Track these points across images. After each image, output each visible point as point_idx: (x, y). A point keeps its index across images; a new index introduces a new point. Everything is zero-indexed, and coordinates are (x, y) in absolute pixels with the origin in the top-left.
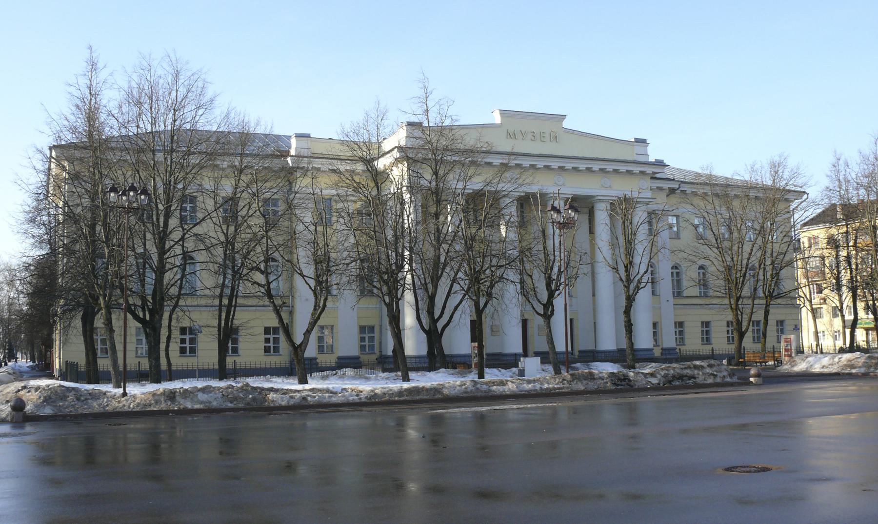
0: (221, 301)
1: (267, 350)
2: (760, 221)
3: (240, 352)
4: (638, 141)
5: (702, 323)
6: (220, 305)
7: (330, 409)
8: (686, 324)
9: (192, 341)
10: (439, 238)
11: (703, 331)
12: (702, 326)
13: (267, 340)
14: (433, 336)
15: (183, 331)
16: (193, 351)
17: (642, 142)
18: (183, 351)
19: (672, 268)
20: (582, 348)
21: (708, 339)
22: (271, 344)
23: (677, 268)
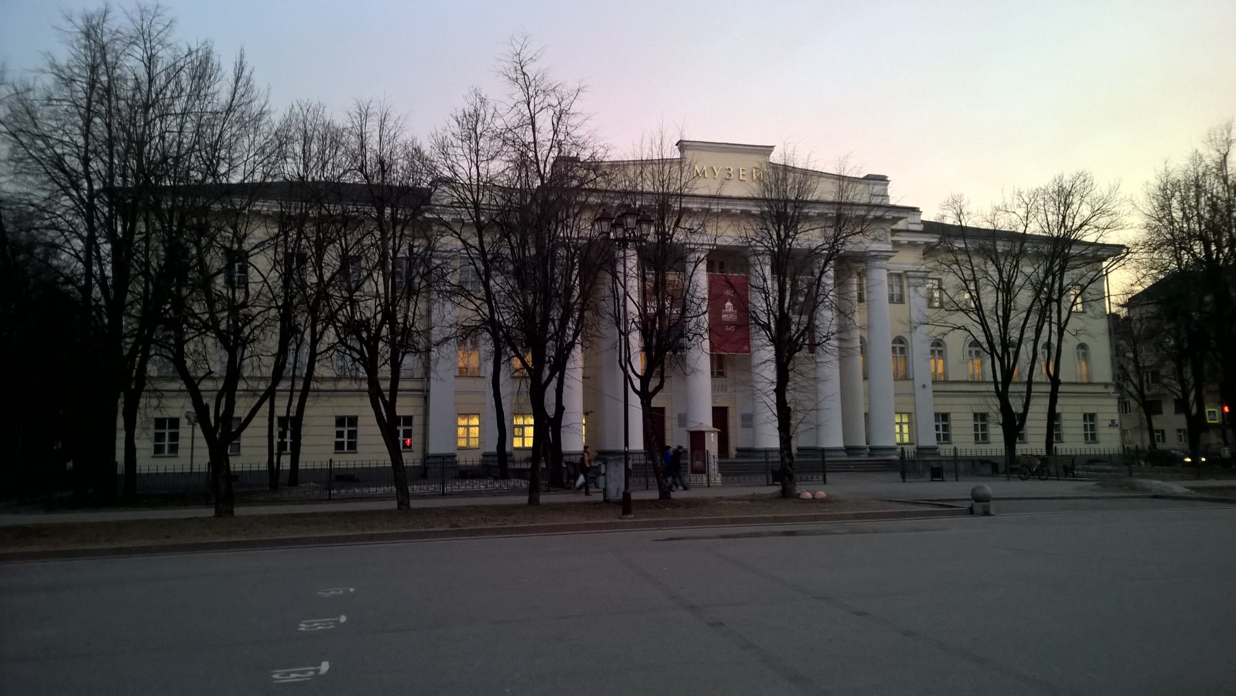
0: (293, 385)
1: (339, 446)
2: (304, 242)
3: (359, 448)
4: (869, 178)
5: (1085, 416)
6: (292, 391)
7: (565, 520)
8: (952, 416)
9: (353, 434)
10: (429, 300)
11: (976, 426)
12: (1085, 420)
13: (340, 434)
14: (901, 428)
15: (160, 423)
16: (352, 446)
17: (882, 179)
18: (158, 450)
19: (894, 342)
20: (741, 446)
21: (1093, 437)
22: (345, 439)
23: (901, 342)
